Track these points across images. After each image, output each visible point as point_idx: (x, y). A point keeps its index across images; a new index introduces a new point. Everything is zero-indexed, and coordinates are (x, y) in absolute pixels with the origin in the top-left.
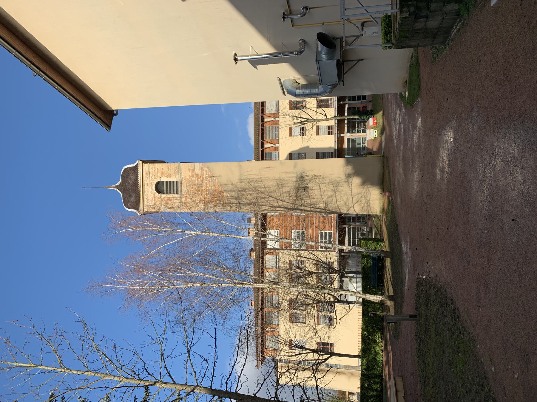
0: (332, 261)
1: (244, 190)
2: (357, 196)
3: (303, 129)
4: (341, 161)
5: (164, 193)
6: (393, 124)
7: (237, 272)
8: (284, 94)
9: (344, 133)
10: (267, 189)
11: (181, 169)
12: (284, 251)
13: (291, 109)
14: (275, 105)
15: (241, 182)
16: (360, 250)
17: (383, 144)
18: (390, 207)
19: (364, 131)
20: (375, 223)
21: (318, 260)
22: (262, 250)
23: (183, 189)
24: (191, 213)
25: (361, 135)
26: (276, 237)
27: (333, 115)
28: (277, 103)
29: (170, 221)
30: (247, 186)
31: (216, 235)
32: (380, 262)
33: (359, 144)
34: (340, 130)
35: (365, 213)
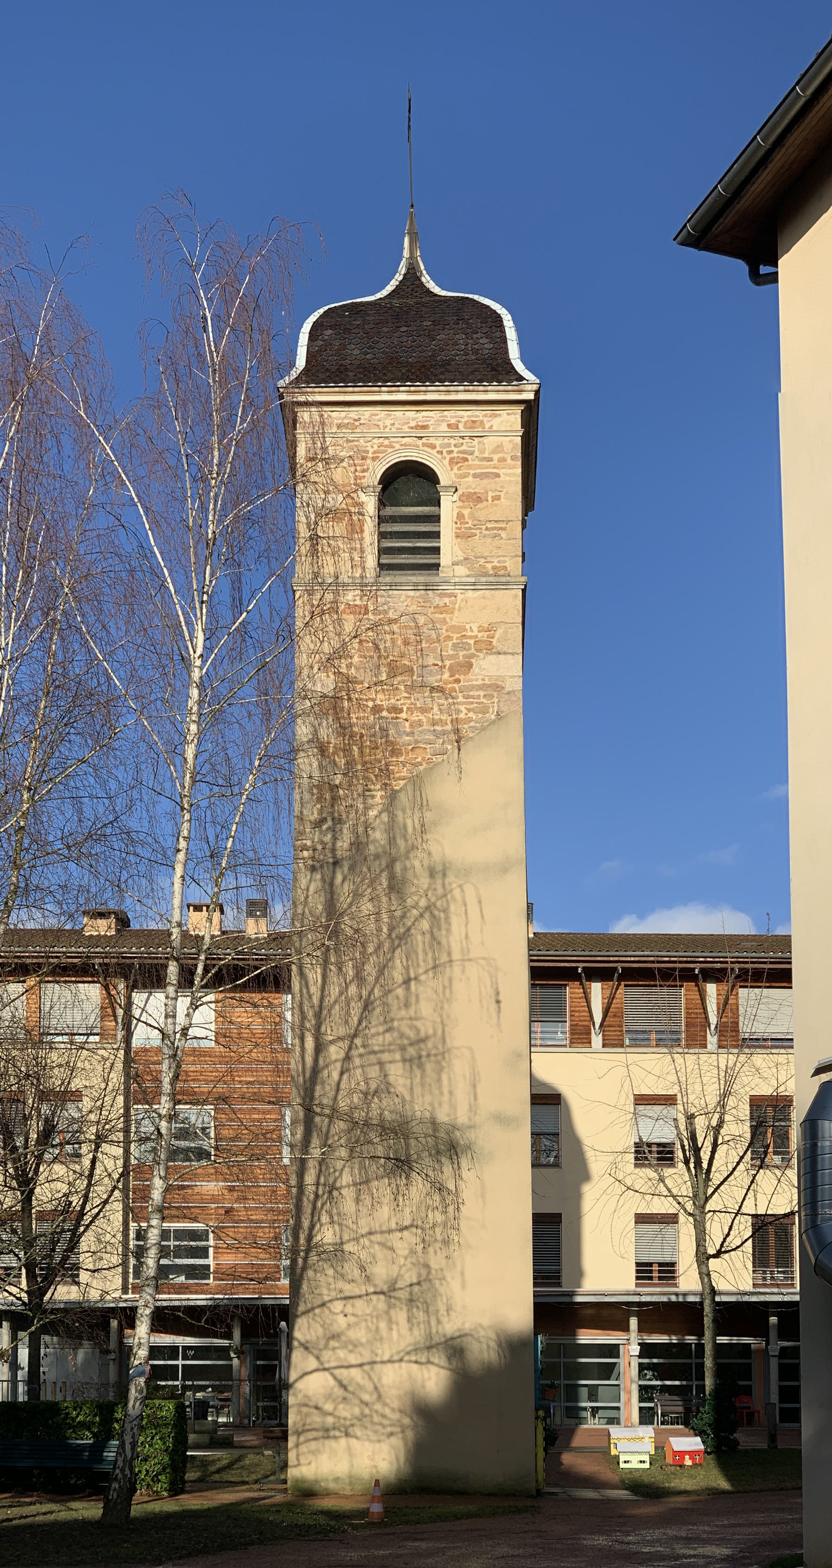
0: (84, 1277)
1: (396, 887)
2: (370, 1386)
3: (663, 1155)
4: (517, 1311)
5: (382, 504)
6: (672, 1532)
7: (20, 849)
8: (818, 1071)
9: (641, 1330)
10: (400, 992)
11: (494, 586)
12: (119, 1065)
13: (756, 1103)
14: (776, 1029)
15: (432, 873)
16: (133, 1393)
17: (590, 1494)
18: (322, 1520)
19: (646, 1417)
20: (250, 1458)
21: (87, 1219)
22: (124, 970)
23: (403, 599)
24: (287, 635)
25: (631, 1404)
26: (185, 1031)
27: (721, 1285)
28: (784, 1043)
29: (254, 532)
30: (416, 898)
31: (190, 752)
32: (80, 1475)
33: (593, 1395)
34: (654, 1316)
35: (292, 1418)
